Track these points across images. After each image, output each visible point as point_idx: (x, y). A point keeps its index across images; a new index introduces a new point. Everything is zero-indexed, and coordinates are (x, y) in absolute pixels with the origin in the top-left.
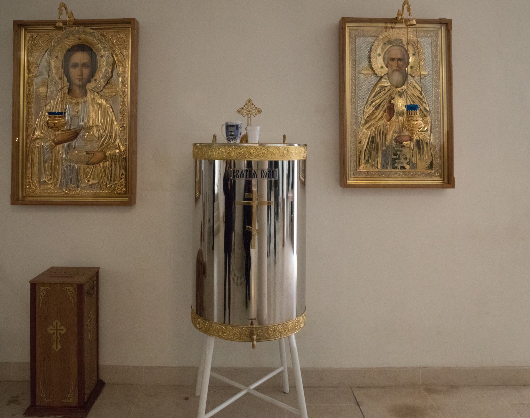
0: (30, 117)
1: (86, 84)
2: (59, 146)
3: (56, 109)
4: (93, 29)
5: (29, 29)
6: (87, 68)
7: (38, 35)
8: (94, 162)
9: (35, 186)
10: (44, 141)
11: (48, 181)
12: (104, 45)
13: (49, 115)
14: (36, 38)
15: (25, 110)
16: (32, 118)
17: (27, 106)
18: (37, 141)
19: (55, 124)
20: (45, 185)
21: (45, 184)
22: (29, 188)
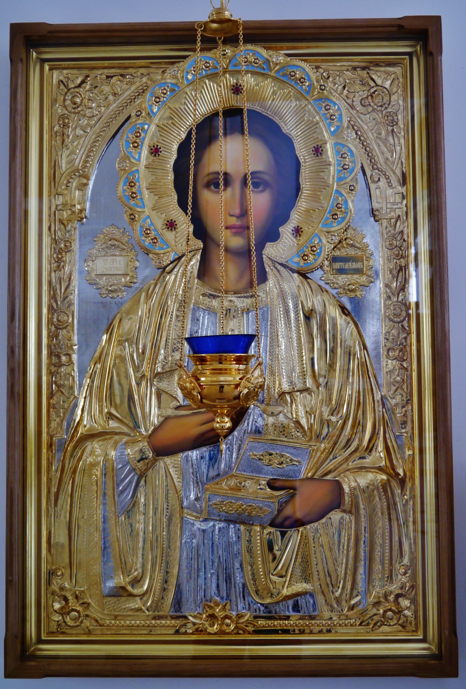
0: (64, 358)
1: (260, 247)
2: (168, 460)
3: (207, 332)
4: (267, 48)
5: (287, 118)
6: (261, 189)
7: (87, 76)
8: (299, 515)
9: (83, 603)
10: (116, 443)
11: (133, 586)
12: (326, 110)
13: (194, 353)
14: (79, 86)
15: (414, 348)
16: (70, 362)
17: (50, 322)
18: (89, 446)
19: (222, 387)
20: (123, 599)
21: (121, 596)
22: (62, 608)
